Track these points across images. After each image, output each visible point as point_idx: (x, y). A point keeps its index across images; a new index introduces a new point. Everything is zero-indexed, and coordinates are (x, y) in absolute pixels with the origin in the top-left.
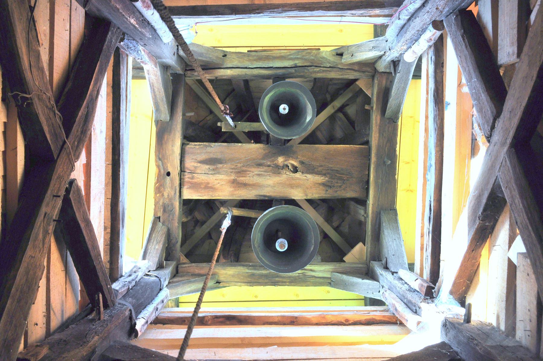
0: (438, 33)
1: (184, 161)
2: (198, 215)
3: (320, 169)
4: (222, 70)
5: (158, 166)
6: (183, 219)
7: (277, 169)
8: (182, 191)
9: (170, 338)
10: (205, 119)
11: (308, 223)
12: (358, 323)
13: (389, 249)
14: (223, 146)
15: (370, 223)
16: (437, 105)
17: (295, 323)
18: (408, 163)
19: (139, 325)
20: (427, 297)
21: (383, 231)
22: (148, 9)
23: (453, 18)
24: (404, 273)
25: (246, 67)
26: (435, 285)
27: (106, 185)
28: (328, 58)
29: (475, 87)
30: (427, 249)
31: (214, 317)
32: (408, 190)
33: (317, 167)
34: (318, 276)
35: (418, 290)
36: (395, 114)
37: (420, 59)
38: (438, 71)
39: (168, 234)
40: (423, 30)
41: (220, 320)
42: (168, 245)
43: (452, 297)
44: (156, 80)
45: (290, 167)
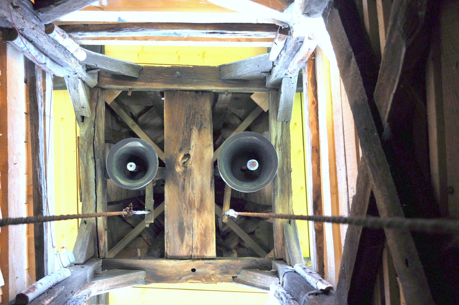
0: (57, 29)
1: (181, 257)
2: (234, 244)
3: (186, 134)
4: (98, 224)
5: (187, 280)
6: (235, 256)
7: (187, 172)
8: (208, 258)
9: (334, 259)
10: (147, 241)
11: (233, 142)
12: (315, 93)
14: (167, 222)
16: (122, 29)
17: (317, 148)
18: (179, 57)
19: (322, 286)
20: (289, 33)
21: (239, 76)
22: (36, 288)
23: (42, 15)
24: (273, 56)
25: (95, 203)
28: (86, 129)
30: (248, 35)
32: (203, 56)
33: (184, 137)
34: (281, 133)
36: (136, 68)
37: (83, 46)
38: (92, 29)
39: (248, 269)
40: (55, 43)
42: (258, 268)
43: (285, 10)
44: (107, 283)
45: (185, 161)
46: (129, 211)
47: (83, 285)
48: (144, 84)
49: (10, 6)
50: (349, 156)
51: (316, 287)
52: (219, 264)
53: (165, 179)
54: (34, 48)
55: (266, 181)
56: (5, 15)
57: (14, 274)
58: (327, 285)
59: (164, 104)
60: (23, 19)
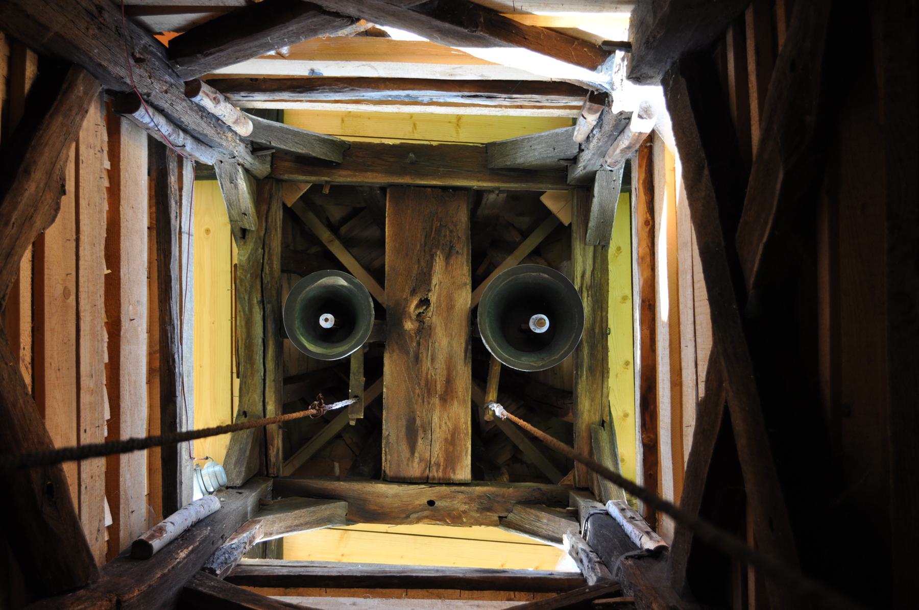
0: (205, 88)
1: (410, 478)
2: (505, 456)
3: (423, 264)
6: (505, 479)
7: (424, 331)
8: (458, 482)
12: (651, 205)
13: (545, 156)
14: (387, 416)
15: (512, 185)
17: (651, 302)
18: (415, 125)
19: (649, 544)
20: (606, 102)
21: (518, 164)
23: (180, 68)
24: (579, 134)
26: (588, 90)
27: (439, 597)
28: (249, 251)
29: (279, 38)
31: (644, 429)
32: (458, 125)
33: (420, 268)
35: (598, 115)
40: (201, 111)
41: (648, 419)
43: (599, 67)
44: (280, 522)
45: (421, 311)
46: (319, 407)
47: (240, 525)
48: (351, 175)
49: (129, 60)
50: (700, 326)
51: (640, 544)
52: (477, 493)
53: (385, 342)
54: (167, 121)
55: (562, 352)
56: (121, 75)
57: (129, 505)
58: (659, 542)
59: (387, 210)
60: (150, 78)
